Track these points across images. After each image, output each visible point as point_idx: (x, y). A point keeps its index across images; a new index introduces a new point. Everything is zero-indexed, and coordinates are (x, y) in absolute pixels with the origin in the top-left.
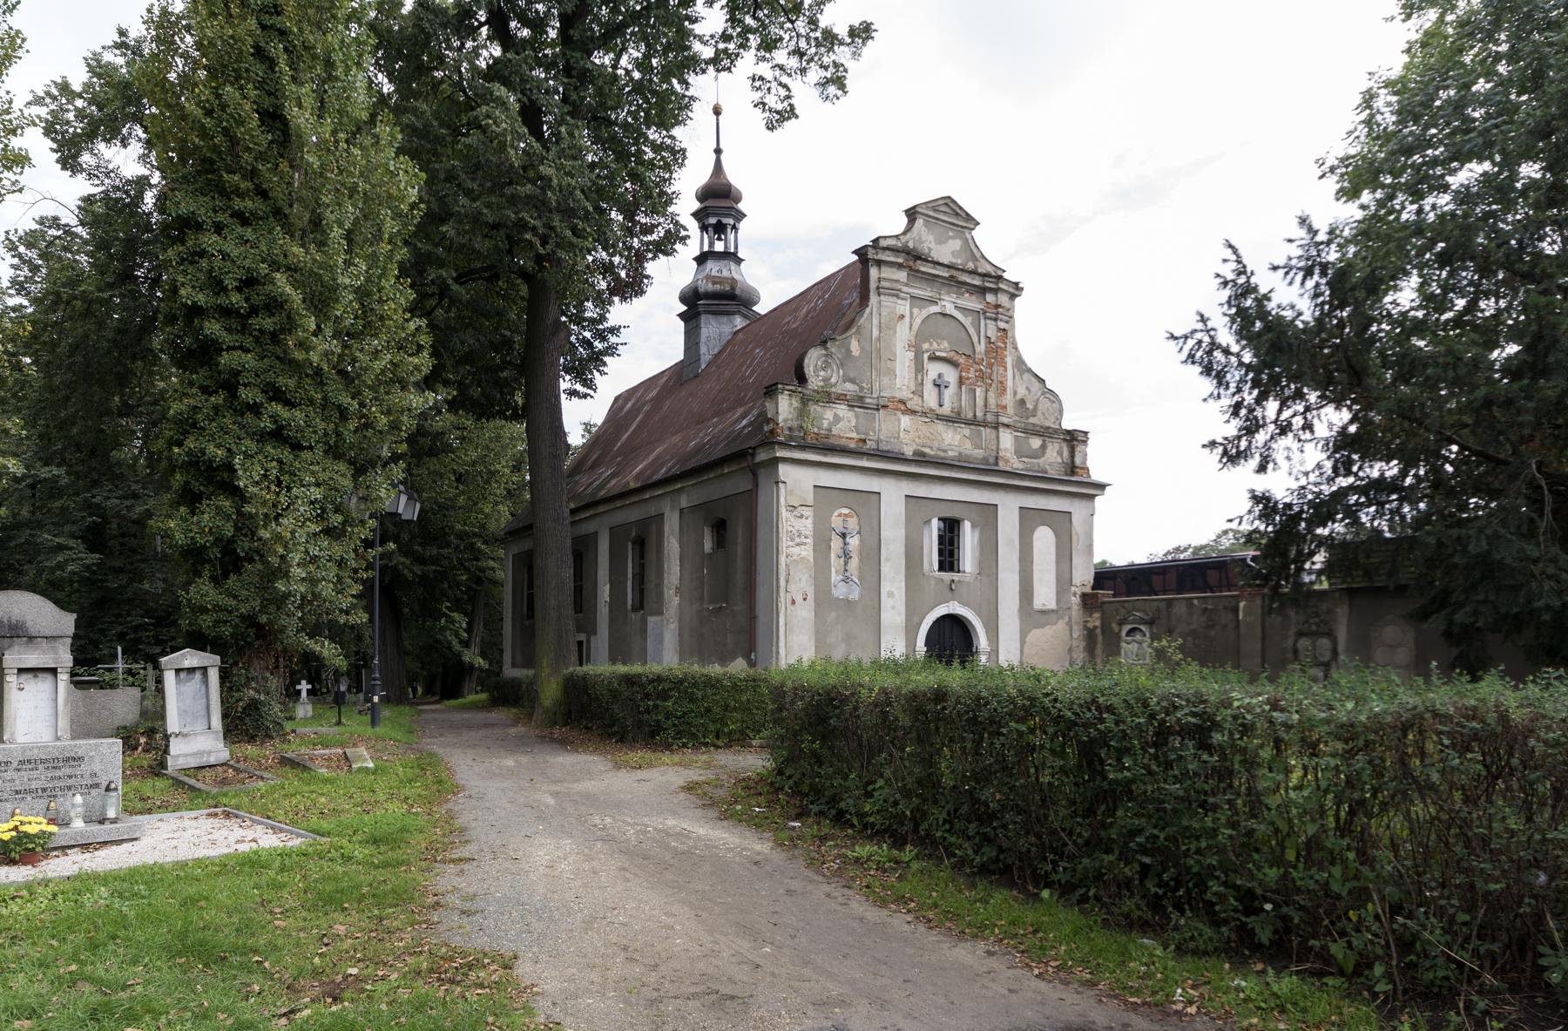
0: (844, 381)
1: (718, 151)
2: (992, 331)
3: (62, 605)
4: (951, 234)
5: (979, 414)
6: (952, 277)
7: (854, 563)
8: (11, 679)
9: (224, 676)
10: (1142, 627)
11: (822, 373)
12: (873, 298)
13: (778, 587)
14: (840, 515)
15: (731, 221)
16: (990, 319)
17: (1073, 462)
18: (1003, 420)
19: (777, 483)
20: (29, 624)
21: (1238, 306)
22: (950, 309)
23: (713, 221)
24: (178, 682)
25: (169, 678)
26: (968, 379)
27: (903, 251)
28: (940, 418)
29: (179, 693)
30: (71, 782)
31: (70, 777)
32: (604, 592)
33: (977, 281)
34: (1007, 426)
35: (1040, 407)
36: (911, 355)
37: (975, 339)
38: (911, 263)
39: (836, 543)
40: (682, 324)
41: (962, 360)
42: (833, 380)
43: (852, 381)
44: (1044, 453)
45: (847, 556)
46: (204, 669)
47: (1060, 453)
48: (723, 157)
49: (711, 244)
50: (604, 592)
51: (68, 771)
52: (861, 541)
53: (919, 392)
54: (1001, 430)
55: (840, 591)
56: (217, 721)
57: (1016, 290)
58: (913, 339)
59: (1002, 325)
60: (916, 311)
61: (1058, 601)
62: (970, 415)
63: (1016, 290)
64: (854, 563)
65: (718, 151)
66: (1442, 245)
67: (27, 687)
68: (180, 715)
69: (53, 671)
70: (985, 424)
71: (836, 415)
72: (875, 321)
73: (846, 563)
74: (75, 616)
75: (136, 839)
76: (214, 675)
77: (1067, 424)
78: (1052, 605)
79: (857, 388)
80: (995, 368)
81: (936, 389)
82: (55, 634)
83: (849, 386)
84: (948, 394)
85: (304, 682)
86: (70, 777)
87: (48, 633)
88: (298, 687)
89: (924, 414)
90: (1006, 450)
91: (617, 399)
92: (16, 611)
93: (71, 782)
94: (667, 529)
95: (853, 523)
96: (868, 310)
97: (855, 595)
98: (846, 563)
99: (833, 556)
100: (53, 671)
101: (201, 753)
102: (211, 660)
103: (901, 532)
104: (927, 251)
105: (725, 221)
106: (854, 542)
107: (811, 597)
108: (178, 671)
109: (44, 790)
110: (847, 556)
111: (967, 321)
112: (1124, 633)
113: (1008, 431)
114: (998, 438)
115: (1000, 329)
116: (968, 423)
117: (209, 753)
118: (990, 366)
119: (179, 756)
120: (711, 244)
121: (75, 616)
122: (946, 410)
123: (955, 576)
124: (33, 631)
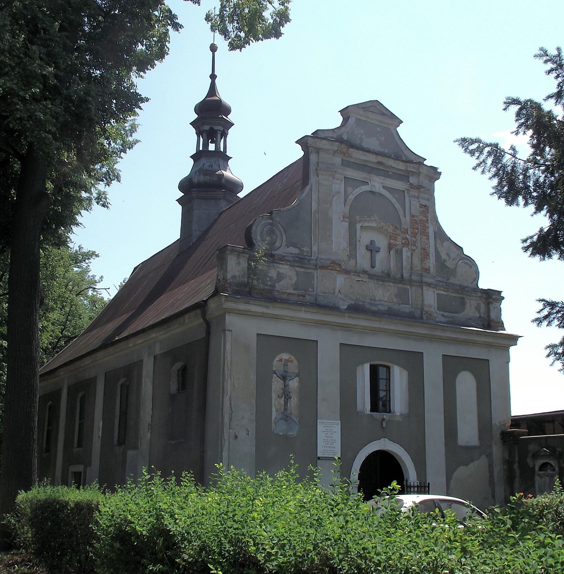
1: (213, 77)
2: (416, 204)
5: (406, 275)
6: (379, 163)
7: (294, 402)
10: (552, 462)
12: (313, 179)
13: (223, 423)
14: (281, 360)
15: (221, 128)
16: (414, 196)
17: (489, 316)
18: (426, 280)
19: (224, 331)
23: (207, 128)
26: (396, 245)
27: (337, 140)
28: (371, 276)
31: (330, 437)
32: (99, 424)
34: (429, 285)
36: (346, 224)
37: (401, 212)
39: (277, 385)
40: (180, 207)
42: (277, 244)
43: (294, 245)
45: (286, 395)
47: (478, 308)
48: (217, 81)
49: (206, 145)
50: (99, 424)
52: (300, 381)
53: (353, 255)
54: (424, 288)
55: (280, 428)
57: (434, 174)
58: (347, 210)
59: (424, 202)
60: (349, 189)
61: (480, 438)
63: (434, 174)
64: (294, 402)
65: (213, 77)
70: (410, 282)
71: (279, 274)
72: (314, 197)
73: (286, 403)
77: (483, 284)
78: (475, 442)
80: (418, 237)
81: (369, 253)
84: (380, 257)
89: (357, 273)
90: (430, 306)
91: (135, 269)
94: (144, 373)
95: (293, 367)
96: (308, 187)
97: (293, 433)
98: (286, 403)
99: (274, 396)
103: (336, 376)
104: (358, 142)
105: (216, 128)
106: (294, 384)
107: (252, 433)
110: (286, 395)
112: (537, 468)
113: (431, 290)
115: (422, 206)
116: (395, 281)
118: (414, 235)
120: (206, 145)
122: (379, 268)
123: (386, 416)
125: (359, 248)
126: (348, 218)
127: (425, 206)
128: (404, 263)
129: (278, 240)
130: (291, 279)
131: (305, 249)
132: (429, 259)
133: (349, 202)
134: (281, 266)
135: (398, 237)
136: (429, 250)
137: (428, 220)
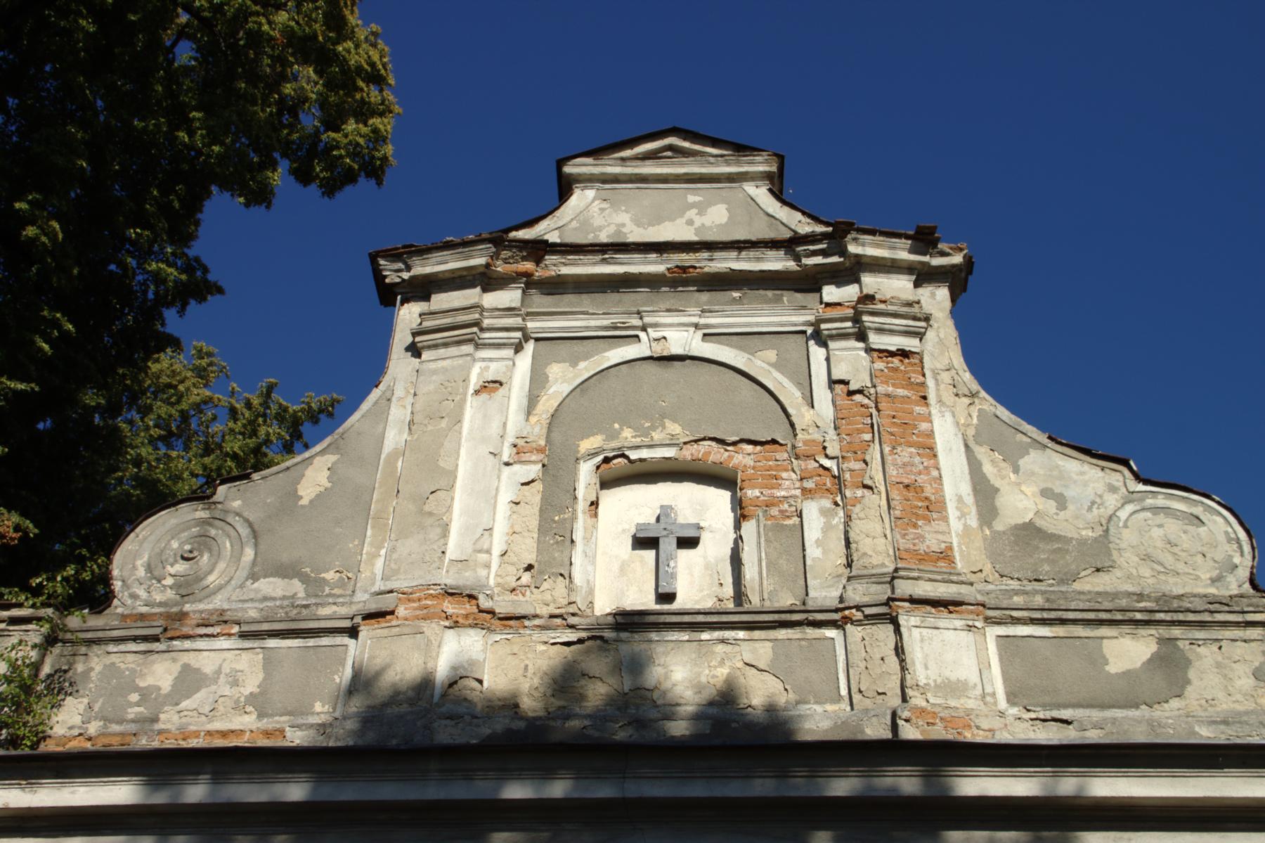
0: (254, 577)
4: (692, 198)
11: (181, 567)
22: (681, 340)
33: (776, 262)
35: (1127, 538)
37: (791, 394)
38: (528, 266)
41: (743, 458)
43: (285, 571)
44: (1178, 686)
62: (787, 600)
70: (839, 618)
79: (297, 587)
83: (272, 587)
111: (761, 364)
114: (899, 651)
125: (587, 539)
126: (540, 450)
127: (904, 354)
128: (813, 552)
129: (221, 565)
130: (235, 683)
131: (330, 576)
132: (945, 519)
133: (547, 404)
134: (201, 644)
135: (784, 475)
136: (940, 490)
137: (925, 398)
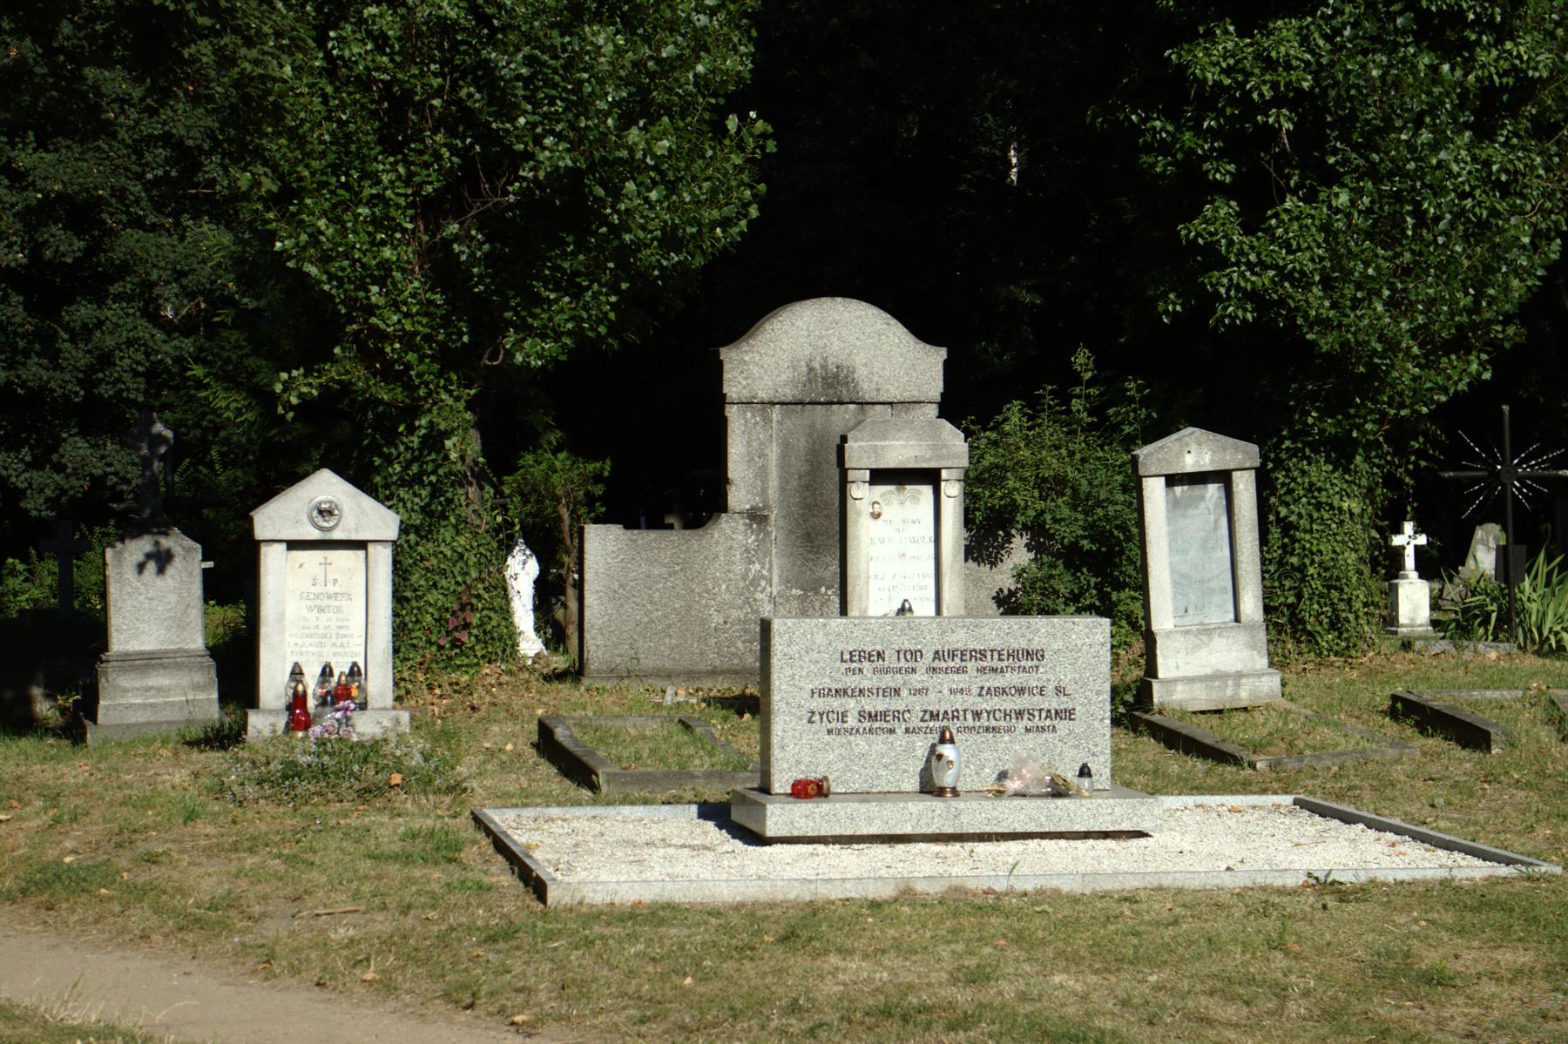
3: (924, 331)
8: (862, 494)
9: (1264, 484)
20: (861, 373)
21: (1058, 555)
24: (1174, 505)
25: (1154, 490)
29: (1173, 536)
30: (1022, 702)
31: (1021, 691)
46: (1223, 477)
51: (1012, 679)
56: (1252, 605)
66: (343, 311)
67: (888, 511)
68: (1176, 584)
69: (930, 477)
74: (943, 353)
75: (1141, 834)
76: (1245, 487)
82: (906, 396)
85: (1409, 527)
86: (1021, 691)
87: (893, 393)
88: (1397, 540)
92: (836, 345)
93: (1022, 702)
100: (930, 477)
101: (1218, 677)
102: (1239, 455)
108: (1172, 480)
109: (977, 715)
117: (1239, 676)
119: (1176, 681)
121: (943, 353)
124: (867, 391)
